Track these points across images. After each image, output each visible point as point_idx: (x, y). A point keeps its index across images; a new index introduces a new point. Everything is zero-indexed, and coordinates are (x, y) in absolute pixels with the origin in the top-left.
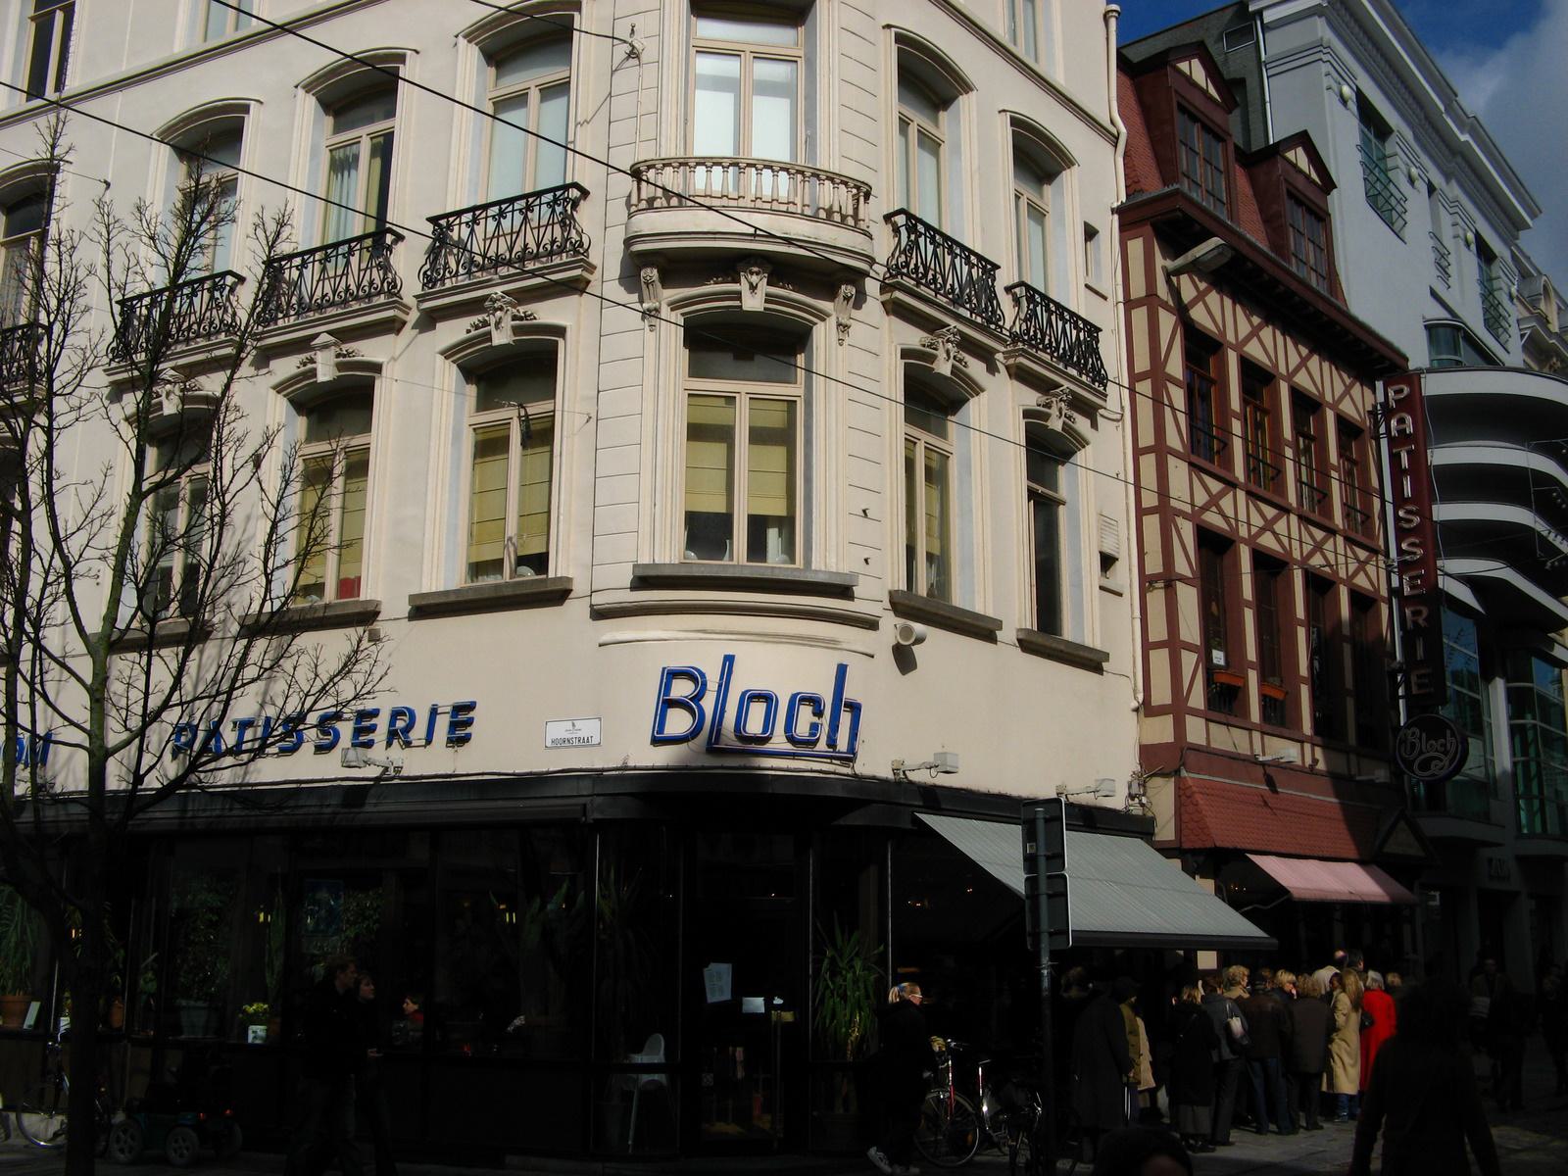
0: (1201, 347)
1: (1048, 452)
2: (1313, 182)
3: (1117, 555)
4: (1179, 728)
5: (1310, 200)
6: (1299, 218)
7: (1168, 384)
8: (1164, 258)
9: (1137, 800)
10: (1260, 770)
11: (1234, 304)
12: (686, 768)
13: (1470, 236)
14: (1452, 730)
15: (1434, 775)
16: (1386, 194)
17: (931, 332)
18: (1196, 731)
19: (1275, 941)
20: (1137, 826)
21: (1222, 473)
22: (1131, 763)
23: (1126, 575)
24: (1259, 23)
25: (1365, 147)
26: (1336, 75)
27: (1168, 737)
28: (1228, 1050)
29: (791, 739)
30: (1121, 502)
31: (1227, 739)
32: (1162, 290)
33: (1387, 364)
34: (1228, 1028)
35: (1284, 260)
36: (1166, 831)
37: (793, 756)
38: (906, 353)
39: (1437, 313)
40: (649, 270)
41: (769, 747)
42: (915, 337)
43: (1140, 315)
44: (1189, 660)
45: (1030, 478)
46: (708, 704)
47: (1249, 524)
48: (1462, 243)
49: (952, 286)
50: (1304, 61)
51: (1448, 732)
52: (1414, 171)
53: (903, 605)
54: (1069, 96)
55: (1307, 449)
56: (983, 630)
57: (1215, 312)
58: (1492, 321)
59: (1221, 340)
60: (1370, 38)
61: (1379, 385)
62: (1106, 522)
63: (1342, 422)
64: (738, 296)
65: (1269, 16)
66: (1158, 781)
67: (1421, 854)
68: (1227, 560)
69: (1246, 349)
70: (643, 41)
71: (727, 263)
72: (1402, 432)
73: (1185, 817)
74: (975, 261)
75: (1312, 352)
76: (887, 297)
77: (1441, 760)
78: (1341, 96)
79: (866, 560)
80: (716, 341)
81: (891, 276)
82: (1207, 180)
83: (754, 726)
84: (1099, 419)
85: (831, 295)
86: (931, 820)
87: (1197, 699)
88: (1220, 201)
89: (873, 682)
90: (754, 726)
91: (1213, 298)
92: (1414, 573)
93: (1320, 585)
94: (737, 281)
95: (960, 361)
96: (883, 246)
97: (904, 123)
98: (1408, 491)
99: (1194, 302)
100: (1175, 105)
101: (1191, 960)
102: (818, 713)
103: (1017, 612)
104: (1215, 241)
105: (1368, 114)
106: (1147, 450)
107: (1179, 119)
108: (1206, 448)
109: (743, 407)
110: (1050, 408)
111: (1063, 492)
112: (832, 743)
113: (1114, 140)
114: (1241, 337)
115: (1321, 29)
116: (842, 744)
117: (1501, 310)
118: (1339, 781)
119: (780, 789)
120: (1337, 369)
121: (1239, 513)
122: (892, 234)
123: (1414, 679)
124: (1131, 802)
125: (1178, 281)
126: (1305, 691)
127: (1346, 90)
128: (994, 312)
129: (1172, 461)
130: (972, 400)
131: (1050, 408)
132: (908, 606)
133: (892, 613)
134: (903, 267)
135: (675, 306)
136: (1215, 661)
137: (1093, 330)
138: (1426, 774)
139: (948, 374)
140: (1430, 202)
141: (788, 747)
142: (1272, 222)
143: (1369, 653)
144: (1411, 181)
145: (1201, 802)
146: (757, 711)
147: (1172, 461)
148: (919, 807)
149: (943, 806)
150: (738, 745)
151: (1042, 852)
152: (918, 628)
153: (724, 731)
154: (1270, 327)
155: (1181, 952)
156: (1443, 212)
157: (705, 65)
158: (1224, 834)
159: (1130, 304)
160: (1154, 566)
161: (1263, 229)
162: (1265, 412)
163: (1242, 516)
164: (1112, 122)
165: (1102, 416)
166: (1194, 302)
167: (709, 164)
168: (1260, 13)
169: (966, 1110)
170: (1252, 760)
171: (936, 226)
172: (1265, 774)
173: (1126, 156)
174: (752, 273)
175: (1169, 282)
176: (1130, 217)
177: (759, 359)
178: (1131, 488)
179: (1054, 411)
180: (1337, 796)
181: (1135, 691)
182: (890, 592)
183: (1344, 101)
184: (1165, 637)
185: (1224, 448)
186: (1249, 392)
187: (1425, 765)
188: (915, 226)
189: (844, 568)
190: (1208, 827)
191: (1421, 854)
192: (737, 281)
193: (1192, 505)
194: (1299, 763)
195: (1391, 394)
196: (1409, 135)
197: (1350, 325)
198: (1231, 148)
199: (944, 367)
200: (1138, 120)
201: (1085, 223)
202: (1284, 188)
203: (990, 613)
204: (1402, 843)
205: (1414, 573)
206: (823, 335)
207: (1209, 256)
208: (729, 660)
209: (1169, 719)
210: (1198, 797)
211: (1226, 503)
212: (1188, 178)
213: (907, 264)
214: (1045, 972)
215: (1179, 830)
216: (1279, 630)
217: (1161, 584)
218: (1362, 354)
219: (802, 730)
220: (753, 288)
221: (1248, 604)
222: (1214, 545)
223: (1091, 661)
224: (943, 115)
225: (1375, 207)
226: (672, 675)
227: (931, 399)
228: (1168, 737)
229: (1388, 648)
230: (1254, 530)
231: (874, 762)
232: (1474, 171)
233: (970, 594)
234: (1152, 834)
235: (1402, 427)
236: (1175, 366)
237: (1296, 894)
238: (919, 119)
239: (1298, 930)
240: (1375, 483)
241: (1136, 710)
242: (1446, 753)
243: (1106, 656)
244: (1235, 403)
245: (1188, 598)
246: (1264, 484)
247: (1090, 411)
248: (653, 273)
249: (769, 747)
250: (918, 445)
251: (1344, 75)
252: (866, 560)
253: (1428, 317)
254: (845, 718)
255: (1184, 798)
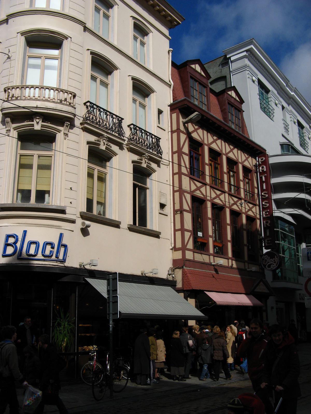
0: (195, 146)
1: (141, 175)
2: (237, 101)
3: (166, 204)
4: (184, 254)
5: (237, 106)
6: (233, 111)
7: (183, 154)
8: (183, 119)
9: (171, 276)
10: (213, 267)
11: (207, 133)
12: (11, 264)
13: (296, 121)
14: (277, 256)
15: (272, 269)
16: (268, 108)
17: (99, 137)
18: (189, 255)
19: (207, 317)
20: (170, 283)
21: (201, 181)
22: (170, 265)
23: (169, 210)
24: (230, 60)
25: (261, 94)
26: (251, 74)
27: (180, 257)
28: (188, 350)
29: (43, 255)
30: (168, 190)
31: (199, 257)
32: (182, 128)
33: (259, 151)
34: (188, 343)
35: (228, 124)
36: (179, 285)
37: (44, 260)
38: (133, 162)
39: (284, 141)
40: (7, 119)
41: (36, 258)
42: (93, 138)
43: (175, 135)
44: (187, 235)
45: (134, 180)
46: (18, 245)
47: (229, 202)
48: (293, 123)
49: (147, 144)
50: (294, 116)
51: (276, 256)
52: (277, 102)
53: (83, 216)
54: (154, 73)
55: (233, 176)
56: (116, 225)
57: (200, 135)
58: (303, 145)
59: (237, 162)
60: (265, 68)
61: (257, 158)
62: (162, 194)
63: (245, 168)
64: (33, 125)
65: (232, 59)
66: (177, 270)
67: (268, 292)
68: (203, 206)
69: (244, 163)
70: (12, 54)
71: (30, 115)
72: (263, 171)
73: (185, 281)
74: (144, 132)
75: (235, 147)
76: (82, 126)
77: (274, 264)
78: (253, 80)
79: (71, 203)
80: (28, 139)
81: (129, 141)
82: (198, 98)
83: (32, 251)
84: (161, 165)
85: (62, 125)
86: (89, 280)
87: (190, 245)
88: (205, 105)
89: (73, 237)
90: (32, 251)
91: (200, 131)
92: (266, 211)
93: (235, 215)
94: (33, 121)
95: (109, 146)
96: (81, 111)
97: (134, 101)
98: (264, 187)
99: (193, 132)
100: (189, 77)
101: (186, 324)
102: (53, 248)
103: (127, 219)
104: (196, 113)
105: (261, 84)
106: (176, 174)
107: (191, 81)
108: (195, 172)
109: (36, 158)
110: (142, 160)
111: (148, 185)
112: (57, 257)
113: (170, 86)
114: (243, 161)
115: (246, 61)
116: (61, 257)
117: (305, 141)
118: (240, 271)
119: (38, 270)
120: (243, 153)
121: (207, 192)
122: (130, 130)
123: (266, 241)
124: (168, 276)
125: (245, 156)
126: (229, 245)
127: (254, 78)
128: (159, 150)
129: (183, 177)
130: (113, 157)
131: (142, 160)
132: (86, 217)
133: (81, 218)
134: (132, 139)
135: (15, 129)
136: (199, 235)
137: (158, 139)
138: (270, 268)
139: (146, 167)
140: (283, 112)
141: (43, 258)
142: (223, 111)
143: (253, 235)
144: (276, 105)
145: (189, 276)
146: (33, 247)
147: (183, 177)
148: (88, 276)
149: (155, 283)
150: (27, 257)
151: (111, 289)
152: (87, 223)
153: (23, 253)
154: (220, 140)
155: (183, 321)
156: (287, 114)
157: (32, 61)
158: (196, 286)
159: (172, 132)
160: (177, 207)
161: (221, 113)
162: (219, 164)
163: (227, 200)
164: (170, 82)
165: (162, 164)
166: (193, 132)
167: (25, 87)
168: (230, 58)
169: (99, 368)
170: (210, 264)
171: (106, 109)
172: (214, 268)
173: (173, 90)
174: (37, 119)
175: (184, 125)
176: (173, 107)
177: (42, 144)
178: (172, 187)
179: (143, 161)
180: (240, 275)
181: (171, 244)
182: (80, 213)
183: (254, 82)
184: (180, 228)
185: (253, 196)
186: (245, 176)
187: (269, 266)
188: (136, 128)
189: (63, 205)
190: (191, 283)
191: (268, 292)
192: (33, 121)
193: (211, 197)
194: (227, 265)
195: (260, 160)
196: (275, 92)
197: (255, 146)
198: (208, 89)
199: (144, 165)
200: (178, 81)
201: (158, 109)
202: (227, 102)
203: (117, 220)
204: (261, 288)
205: (266, 211)
206: (59, 137)
207: (195, 117)
208: (25, 232)
209: (181, 252)
210: (188, 274)
211: (254, 210)
212: (231, 121)
213: (134, 138)
214: (111, 326)
215: (183, 285)
216: (222, 227)
217: (179, 212)
218: (255, 150)
219: (47, 252)
220: (38, 123)
221: (210, 219)
222: (198, 202)
223: (156, 235)
224: (109, 77)
225: (265, 112)
226: (8, 236)
227: (98, 157)
228: (180, 257)
229: (259, 233)
230: (247, 210)
231: (73, 262)
232: (296, 103)
233: (112, 214)
234: (176, 286)
235: (263, 169)
236: (186, 149)
237: (218, 303)
238: (139, 99)
239: (217, 315)
240: (256, 185)
241: (172, 249)
242: (275, 262)
243: (160, 233)
244: (207, 161)
245: (188, 217)
246: (217, 184)
247: (158, 163)
248: (8, 119)
249: (36, 258)
250: (95, 170)
251: (253, 74)
252: (71, 203)
253: (281, 142)
254: (62, 249)
255: (184, 275)
